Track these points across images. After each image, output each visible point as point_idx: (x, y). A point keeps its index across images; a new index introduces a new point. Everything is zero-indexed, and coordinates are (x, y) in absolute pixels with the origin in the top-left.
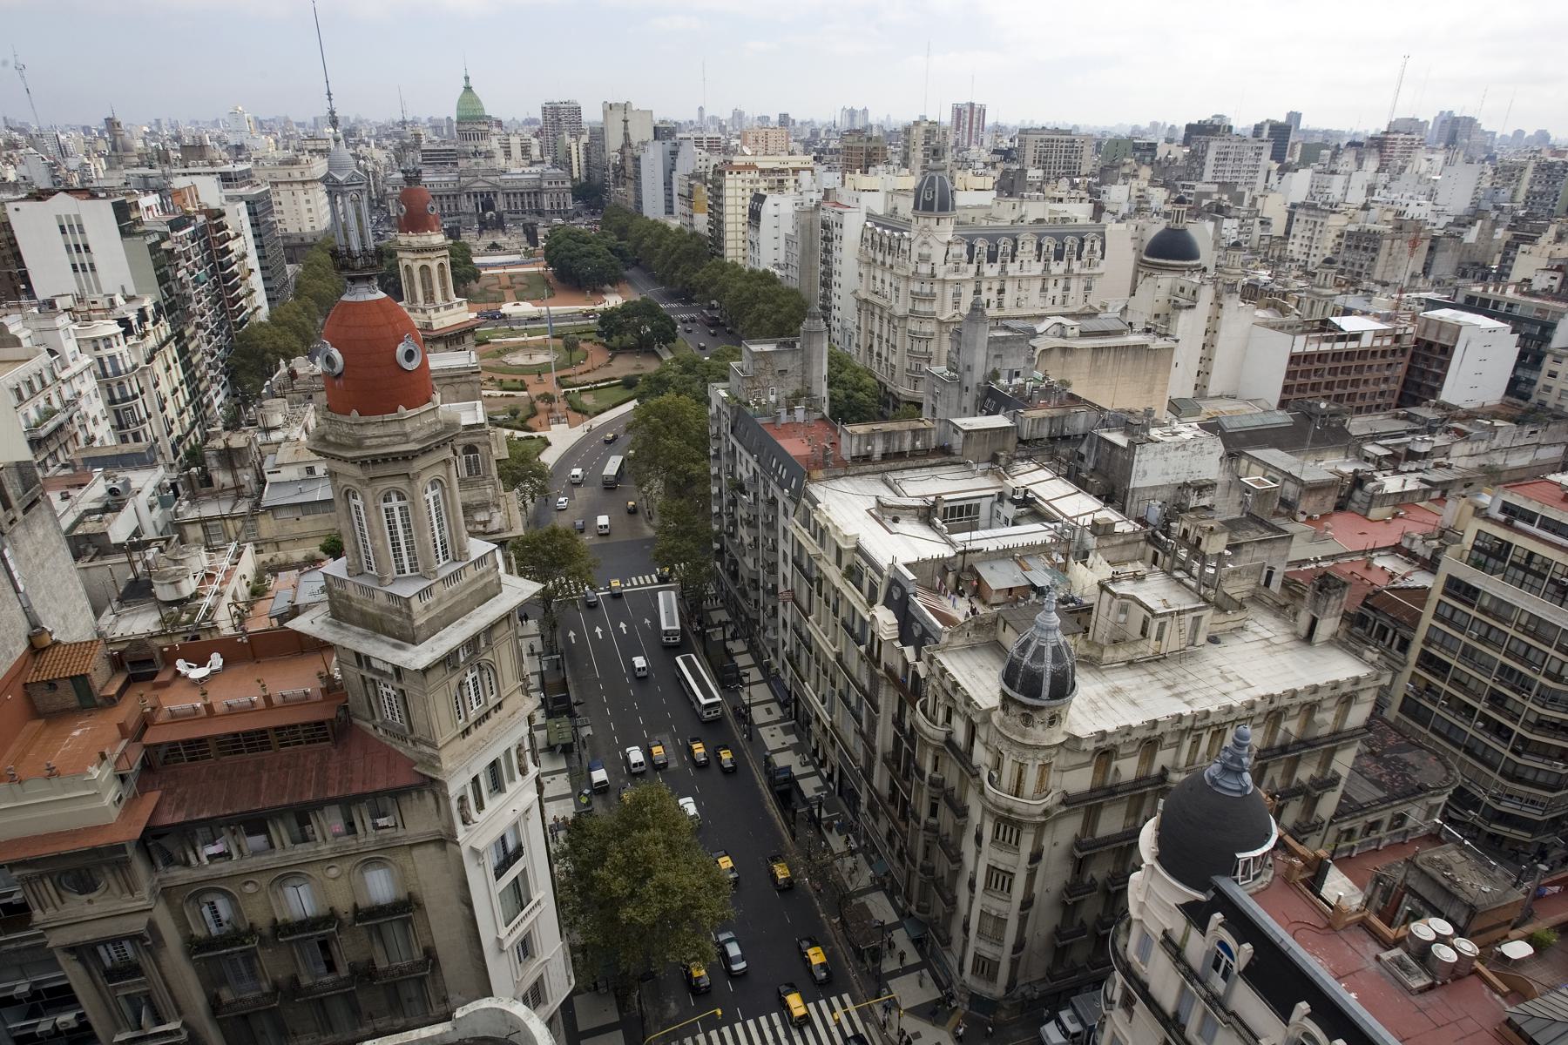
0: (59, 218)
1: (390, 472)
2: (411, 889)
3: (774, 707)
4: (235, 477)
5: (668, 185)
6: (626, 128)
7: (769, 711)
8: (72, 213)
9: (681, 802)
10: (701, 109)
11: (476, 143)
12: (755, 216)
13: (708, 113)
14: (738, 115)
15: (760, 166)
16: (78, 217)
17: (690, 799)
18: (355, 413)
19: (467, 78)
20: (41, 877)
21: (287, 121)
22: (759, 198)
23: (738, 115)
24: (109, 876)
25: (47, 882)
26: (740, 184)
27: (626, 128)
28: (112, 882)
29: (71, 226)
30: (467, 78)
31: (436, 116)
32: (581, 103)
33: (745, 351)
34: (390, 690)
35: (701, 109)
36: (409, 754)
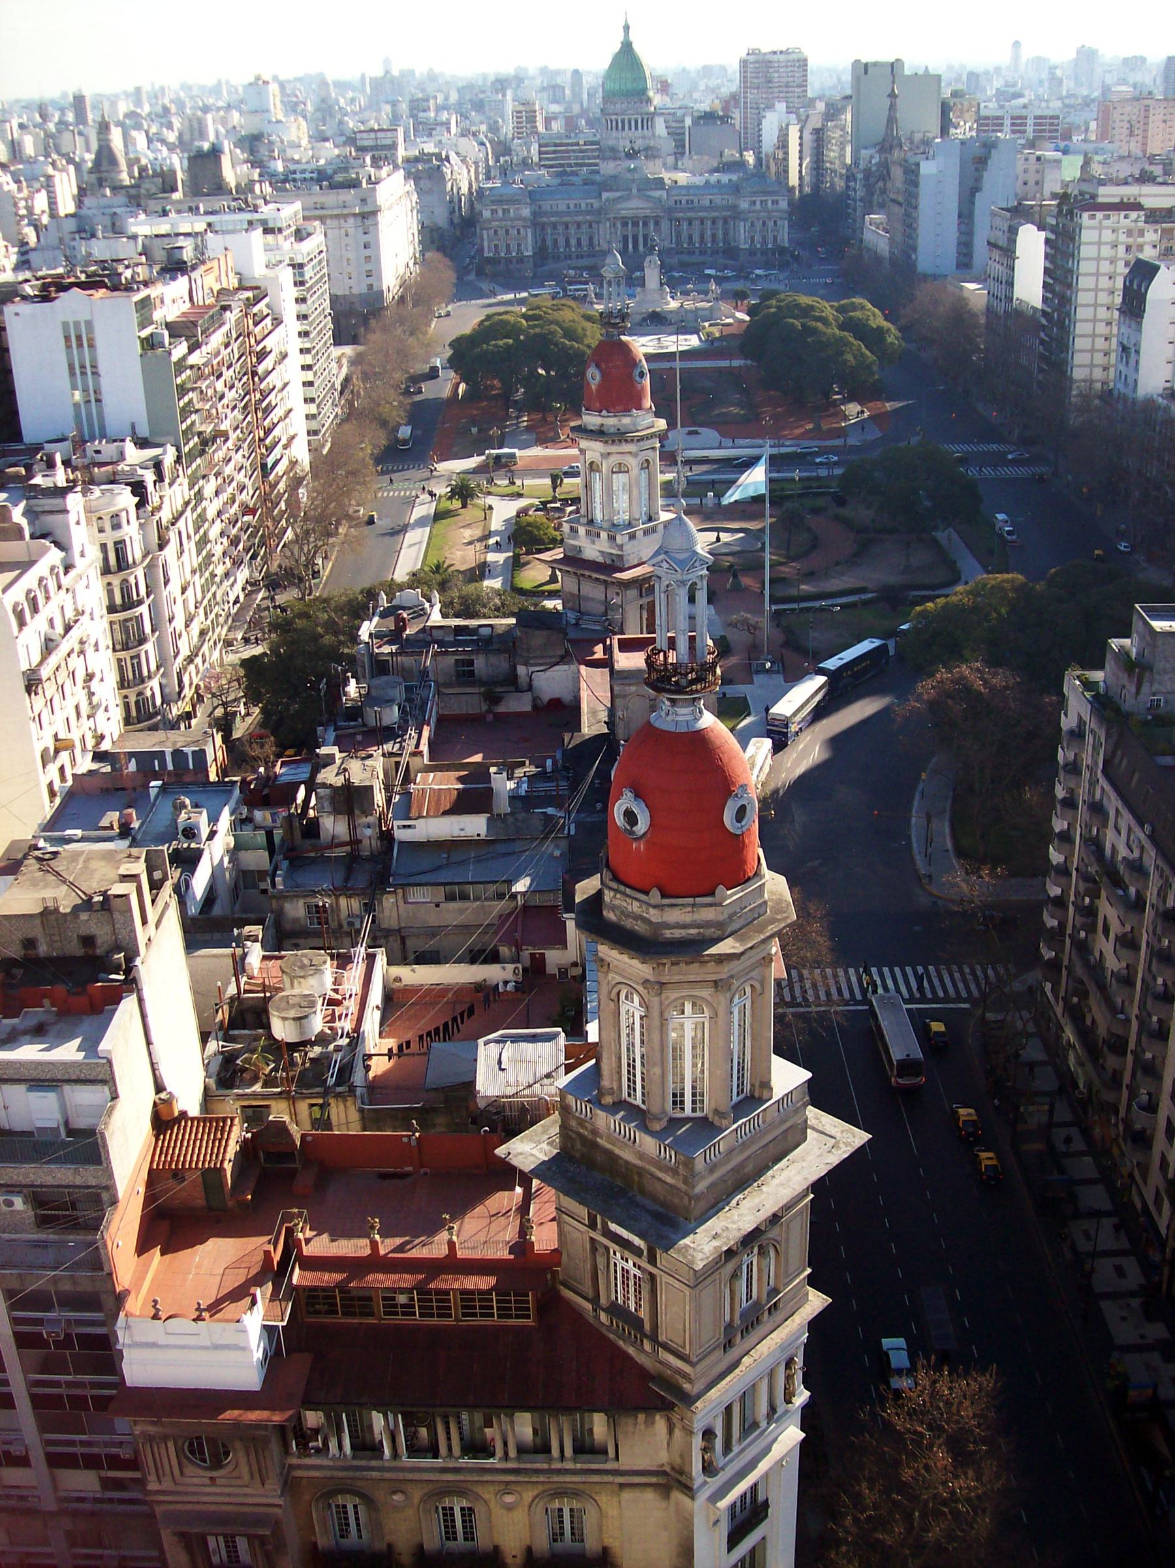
0: (65, 325)
1: (692, 978)
2: (608, 1542)
3: (1131, 1265)
4: (352, 827)
5: (966, 216)
6: (892, 107)
7: (1120, 1271)
8: (82, 317)
9: (887, 1342)
10: (1017, 44)
11: (632, 134)
12: (1133, 304)
13: (1027, 54)
14: (1087, 56)
15: (1148, 203)
16: (89, 324)
17: (901, 1342)
18: (655, 892)
19: (627, 28)
20: (165, 1438)
21: (324, 83)
22: (1142, 273)
23: (1087, 56)
24: (241, 1454)
25: (171, 1444)
26: (1107, 236)
27: (892, 107)
28: (243, 1460)
29: (79, 338)
30: (627, 28)
31: (553, 66)
32: (807, 52)
33: (1136, 624)
34: (629, 1265)
35: (1017, 44)
36: (641, 1359)
